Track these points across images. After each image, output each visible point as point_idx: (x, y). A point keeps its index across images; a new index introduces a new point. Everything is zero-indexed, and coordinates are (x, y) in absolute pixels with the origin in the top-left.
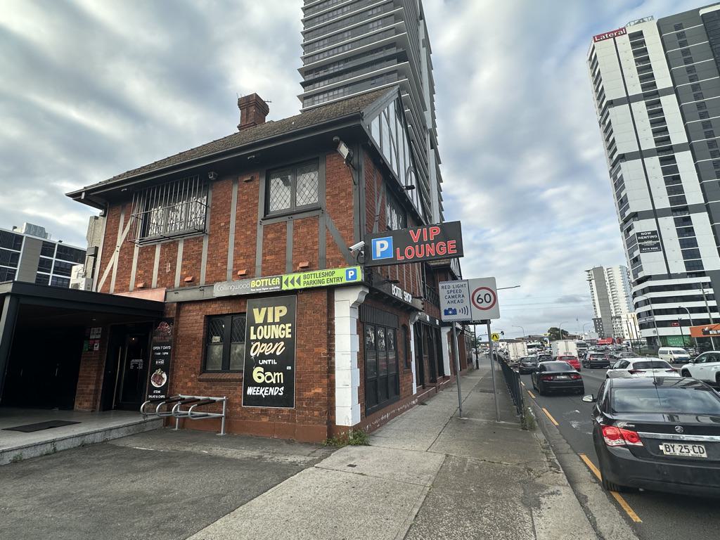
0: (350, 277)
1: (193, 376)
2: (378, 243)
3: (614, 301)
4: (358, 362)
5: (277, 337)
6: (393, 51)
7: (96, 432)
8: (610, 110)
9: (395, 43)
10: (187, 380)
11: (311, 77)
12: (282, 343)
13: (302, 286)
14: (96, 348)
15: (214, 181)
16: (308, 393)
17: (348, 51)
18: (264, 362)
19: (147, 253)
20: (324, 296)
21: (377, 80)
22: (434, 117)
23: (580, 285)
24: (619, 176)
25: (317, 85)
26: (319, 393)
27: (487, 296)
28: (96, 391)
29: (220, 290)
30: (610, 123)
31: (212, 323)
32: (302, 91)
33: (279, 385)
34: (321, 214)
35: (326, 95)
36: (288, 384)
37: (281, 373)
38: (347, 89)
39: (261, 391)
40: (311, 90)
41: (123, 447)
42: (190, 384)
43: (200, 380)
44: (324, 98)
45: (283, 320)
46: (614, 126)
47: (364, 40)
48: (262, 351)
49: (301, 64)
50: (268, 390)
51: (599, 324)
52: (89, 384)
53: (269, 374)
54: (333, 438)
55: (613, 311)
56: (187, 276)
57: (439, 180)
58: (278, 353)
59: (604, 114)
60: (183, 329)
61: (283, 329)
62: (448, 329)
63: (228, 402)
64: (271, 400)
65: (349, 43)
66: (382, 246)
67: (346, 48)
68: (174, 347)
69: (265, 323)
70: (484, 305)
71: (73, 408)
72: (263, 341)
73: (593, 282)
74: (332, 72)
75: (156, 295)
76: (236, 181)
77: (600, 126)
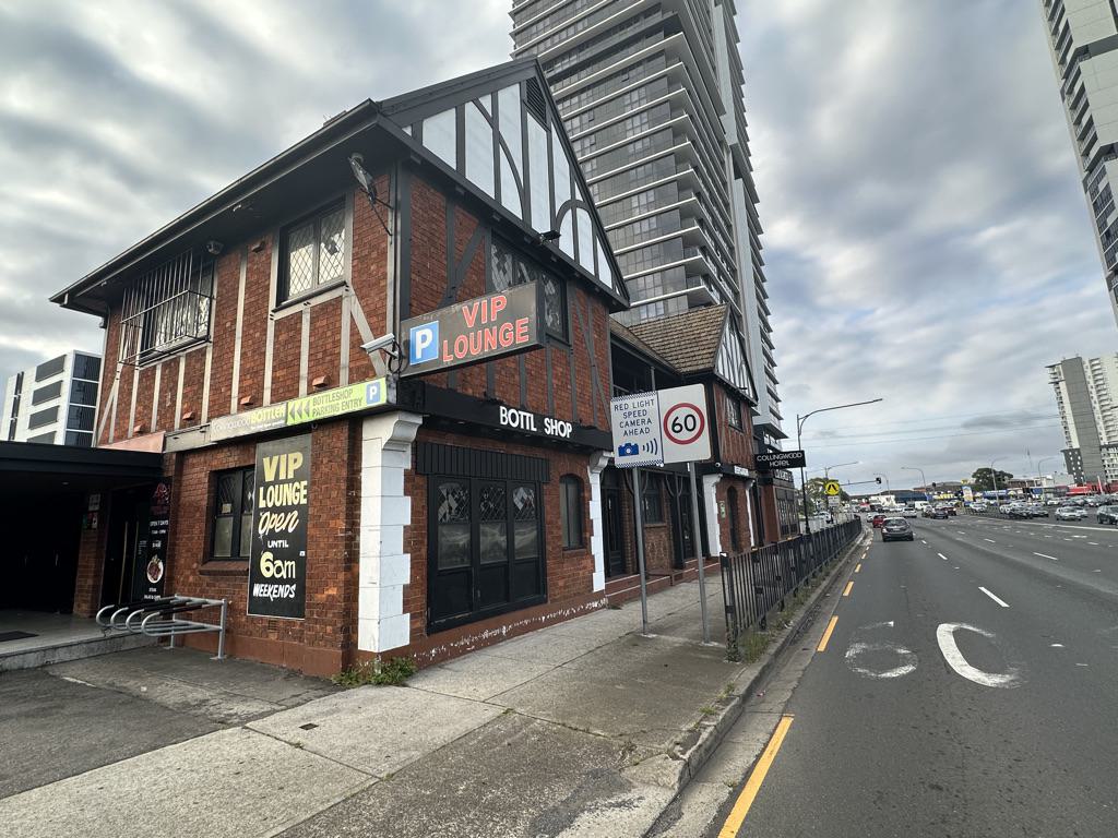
0: (371, 398)
1: (195, 565)
2: (419, 335)
3: (1106, 422)
5: (290, 504)
6: (657, 18)
7: (25, 653)
8: (1084, 65)
10: (188, 573)
12: (296, 513)
13: (311, 418)
14: (95, 525)
16: (319, 596)
17: (583, 31)
18: (274, 544)
19: (148, 377)
20: (343, 433)
22: (741, 124)
23: (1037, 392)
24: (1101, 187)
26: (333, 596)
27: (690, 419)
28: (95, 587)
29: (222, 429)
30: (1083, 89)
31: (219, 478)
33: (289, 581)
34: (345, 293)
36: (299, 580)
37: (293, 563)
38: (584, 96)
39: (270, 590)
41: (53, 676)
42: (191, 579)
43: (202, 573)
45: (298, 476)
46: (1090, 95)
47: (606, 9)
48: (271, 527)
50: (277, 589)
51: (1076, 460)
52: (87, 577)
53: (278, 563)
54: (350, 668)
55: (1104, 436)
56: (187, 411)
57: (755, 228)
58: (290, 530)
59: (1070, 73)
60: (186, 494)
61: (298, 490)
62: (715, 479)
63: (230, 607)
64: (280, 606)
65: (585, 18)
66: (424, 338)
67: (580, 26)
68: (175, 523)
69: (277, 482)
70: (685, 435)
71: (72, 612)
72: (275, 510)
73: (1062, 385)
74: (560, 70)
75: (151, 444)
76: (245, 255)
77: (1063, 99)
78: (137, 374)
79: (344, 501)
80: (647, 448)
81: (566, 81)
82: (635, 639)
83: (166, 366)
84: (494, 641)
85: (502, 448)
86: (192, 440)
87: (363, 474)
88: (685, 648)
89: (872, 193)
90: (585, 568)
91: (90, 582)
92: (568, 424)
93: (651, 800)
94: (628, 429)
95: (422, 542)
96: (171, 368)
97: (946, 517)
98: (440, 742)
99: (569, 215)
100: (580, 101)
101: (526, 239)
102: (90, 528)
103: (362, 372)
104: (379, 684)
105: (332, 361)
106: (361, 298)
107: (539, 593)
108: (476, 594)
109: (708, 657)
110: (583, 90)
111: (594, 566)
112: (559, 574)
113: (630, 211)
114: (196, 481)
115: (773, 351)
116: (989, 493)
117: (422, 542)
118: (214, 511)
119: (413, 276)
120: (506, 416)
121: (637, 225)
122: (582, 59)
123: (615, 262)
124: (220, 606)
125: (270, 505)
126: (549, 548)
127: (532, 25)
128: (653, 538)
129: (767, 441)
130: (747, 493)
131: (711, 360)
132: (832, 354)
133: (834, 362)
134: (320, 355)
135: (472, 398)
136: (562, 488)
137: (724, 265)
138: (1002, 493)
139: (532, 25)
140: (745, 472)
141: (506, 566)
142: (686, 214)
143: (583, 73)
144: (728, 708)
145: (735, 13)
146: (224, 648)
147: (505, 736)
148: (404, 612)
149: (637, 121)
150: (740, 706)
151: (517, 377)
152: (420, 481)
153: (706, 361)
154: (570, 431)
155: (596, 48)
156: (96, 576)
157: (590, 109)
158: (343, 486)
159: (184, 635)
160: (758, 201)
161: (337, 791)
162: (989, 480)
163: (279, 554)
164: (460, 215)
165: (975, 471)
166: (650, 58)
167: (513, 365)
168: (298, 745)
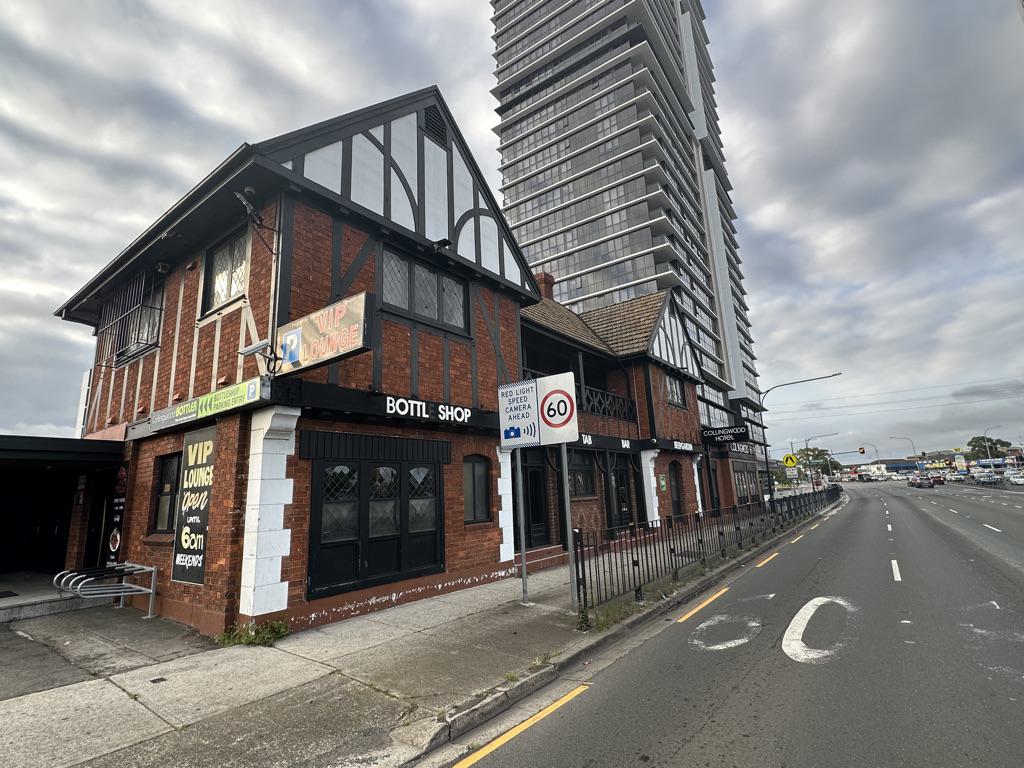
4: (285, 520)
6: (624, 30)
9: (625, 17)
10: (137, 543)
11: (509, 98)
14: (81, 501)
15: (166, 274)
17: (557, 47)
18: (191, 520)
21: (601, 81)
22: (712, 119)
25: (518, 107)
27: (562, 404)
29: (161, 420)
31: (163, 461)
32: (497, 120)
35: (530, 120)
38: (559, 105)
40: (512, 115)
42: (139, 549)
43: (145, 543)
45: (210, 461)
49: (494, 83)
52: (74, 545)
53: (193, 536)
54: (232, 629)
58: (202, 508)
62: (653, 454)
63: (160, 574)
67: (554, 43)
70: (558, 420)
72: (194, 490)
75: (116, 434)
78: (113, 373)
79: (234, 483)
80: (527, 431)
81: (543, 93)
82: (514, 606)
83: (131, 367)
84: (347, 616)
85: (397, 434)
86: (143, 430)
87: (250, 460)
88: (552, 617)
89: (858, 173)
90: (490, 540)
91: (76, 549)
92: (466, 410)
93: (402, 753)
94: (512, 414)
95: (305, 519)
96: (134, 368)
97: (932, 486)
98: (251, 699)
99: (469, 226)
100: (555, 110)
101: (419, 248)
102: (78, 504)
103: (251, 372)
104: (251, 644)
105: (233, 363)
106: (254, 308)
107: (436, 563)
109: (563, 625)
110: (557, 100)
111: (502, 539)
112: (458, 546)
114: (146, 465)
116: (984, 461)
117: (305, 519)
118: (158, 490)
119: (293, 288)
120: (393, 406)
122: (556, 72)
123: (521, 255)
124: (151, 572)
125: (190, 486)
126: (448, 522)
127: (512, 46)
128: (582, 511)
129: (744, 414)
130: (695, 467)
131: (646, 343)
132: (824, 328)
133: (825, 336)
134: (226, 358)
136: (467, 469)
137: (695, 251)
138: (999, 461)
139: (512, 46)
140: (689, 447)
141: (397, 539)
142: (654, 205)
143: (557, 84)
144: (535, 675)
145: (704, 18)
146: (155, 608)
147: (313, 694)
148: (282, 580)
149: (607, 123)
150: (552, 673)
151: (408, 370)
152: (304, 465)
153: (641, 344)
154: (469, 415)
155: (564, 63)
156: (80, 545)
157: (565, 116)
158: (234, 470)
159: (132, 596)
161: (136, 736)
162: (982, 448)
163: (194, 529)
164: (347, 230)
165: (970, 439)
166: (617, 67)
167: (404, 360)
168: (135, 698)
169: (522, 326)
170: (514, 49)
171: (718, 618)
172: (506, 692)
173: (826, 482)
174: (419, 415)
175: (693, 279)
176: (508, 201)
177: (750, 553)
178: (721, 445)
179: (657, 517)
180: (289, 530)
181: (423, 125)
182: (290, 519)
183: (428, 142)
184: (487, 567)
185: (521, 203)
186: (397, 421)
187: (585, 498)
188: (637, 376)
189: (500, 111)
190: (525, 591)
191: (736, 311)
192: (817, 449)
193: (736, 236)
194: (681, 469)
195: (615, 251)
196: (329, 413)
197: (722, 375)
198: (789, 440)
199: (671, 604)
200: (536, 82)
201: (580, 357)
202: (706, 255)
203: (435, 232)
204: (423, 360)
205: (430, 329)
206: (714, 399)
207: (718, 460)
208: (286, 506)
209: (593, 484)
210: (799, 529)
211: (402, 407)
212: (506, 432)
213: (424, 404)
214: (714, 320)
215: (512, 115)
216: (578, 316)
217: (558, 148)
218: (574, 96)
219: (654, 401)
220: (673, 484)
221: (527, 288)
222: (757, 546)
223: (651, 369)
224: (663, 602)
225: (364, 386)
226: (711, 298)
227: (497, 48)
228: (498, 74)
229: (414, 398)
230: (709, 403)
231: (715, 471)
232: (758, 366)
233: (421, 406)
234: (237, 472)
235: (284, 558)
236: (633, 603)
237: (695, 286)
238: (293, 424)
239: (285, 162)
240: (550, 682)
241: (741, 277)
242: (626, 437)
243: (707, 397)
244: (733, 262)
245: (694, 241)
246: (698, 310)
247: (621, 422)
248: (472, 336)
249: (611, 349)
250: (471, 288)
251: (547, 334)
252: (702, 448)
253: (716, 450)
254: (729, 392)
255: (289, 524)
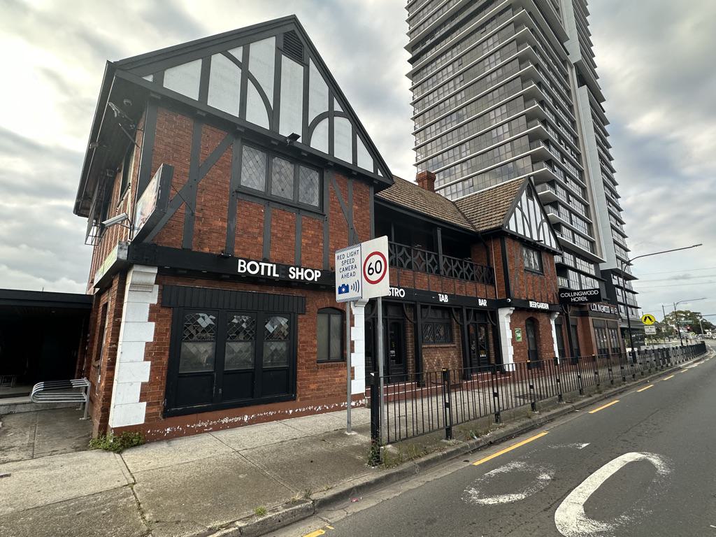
11: (418, 50)
21: (488, 27)
27: (378, 263)
32: (410, 68)
35: (434, 64)
38: (455, 50)
40: (420, 63)
44: (436, 65)
49: (407, 41)
62: (509, 311)
70: (375, 277)
84: (201, 431)
92: (316, 272)
95: (164, 354)
98: (40, 503)
108: (217, 391)
112: (309, 381)
113: (490, 121)
115: (616, 187)
117: (164, 354)
120: (243, 267)
121: (494, 131)
126: (301, 361)
129: (615, 282)
130: (553, 323)
132: (698, 211)
133: (701, 218)
135: (210, 255)
136: (322, 320)
137: (568, 152)
140: (545, 306)
148: (141, 401)
149: (492, 58)
150: (308, 510)
152: (165, 311)
153: (498, 221)
154: (319, 275)
155: (456, 19)
160: (604, 100)
164: (207, 130)
169: (375, 203)
170: (421, 14)
171: (517, 465)
172: (240, 528)
173: (693, 339)
174: (269, 274)
175: (566, 174)
176: (417, 126)
177: (591, 398)
178: (578, 305)
179: (511, 361)
180: (150, 362)
181: (282, 46)
182: (150, 354)
183: (287, 62)
184: (338, 398)
185: (427, 127)
186: (248, 279)
187: (442, 346)
188: (495, 248)
189: (411, 61)
190: (349, 422)
191: (608, 198)
192: (689, 312)
193: (608, 139)
194: (539, 324)
195: (500, 156)
196: (324, 287)
197: (593, 250)
198: (661, 304)
199: (481, 444)
200: (438, 35)
201: (439, 232)
202: (579, 155)
203: (290, 126)
204: (276, 231)
205: (283, 207)
206: (587, 271)
207: (578, 318)
208: (147, 343)
209: (452, 335)
210: (651, 380)
211: (253, 268)
212: (340, 289)
213: (275, 266)
214: (587, 206)
215: (420, 63)
216: (453, 203)
217: (455, 83)
218: (463, 44)
219: (510, 267)
220: (531, 336)
221: (380, 174)
222: (600, 392)
223: (508, 242)
224: (472, 442)
225: (217, 250)
226: (584, 189)
227: (409, 15)
228: (410, 34)
229: (264, 261)
230: (580, 272)
231: (575, 327)
232: (628, 243)
233: (272, 268)
234: (115, 316)
235: (143, 384)
236: (444, 441)
237: (568, 179)
238: (153, 279)
239: (146, 75)
240: (304, 519)
241: (613, 171)
242: (483, 296)
243: (579, 267)
244: (605, 159)
245: (567, 144)
246: (571, 198)
247: (479, 286)
248: (325, 212)
249: (474, 227)
250: (325, 174)
251: (383, 204)
252: (558, 307)
253: (577, 309)
254: (600, 264)
255: (150, 358)
